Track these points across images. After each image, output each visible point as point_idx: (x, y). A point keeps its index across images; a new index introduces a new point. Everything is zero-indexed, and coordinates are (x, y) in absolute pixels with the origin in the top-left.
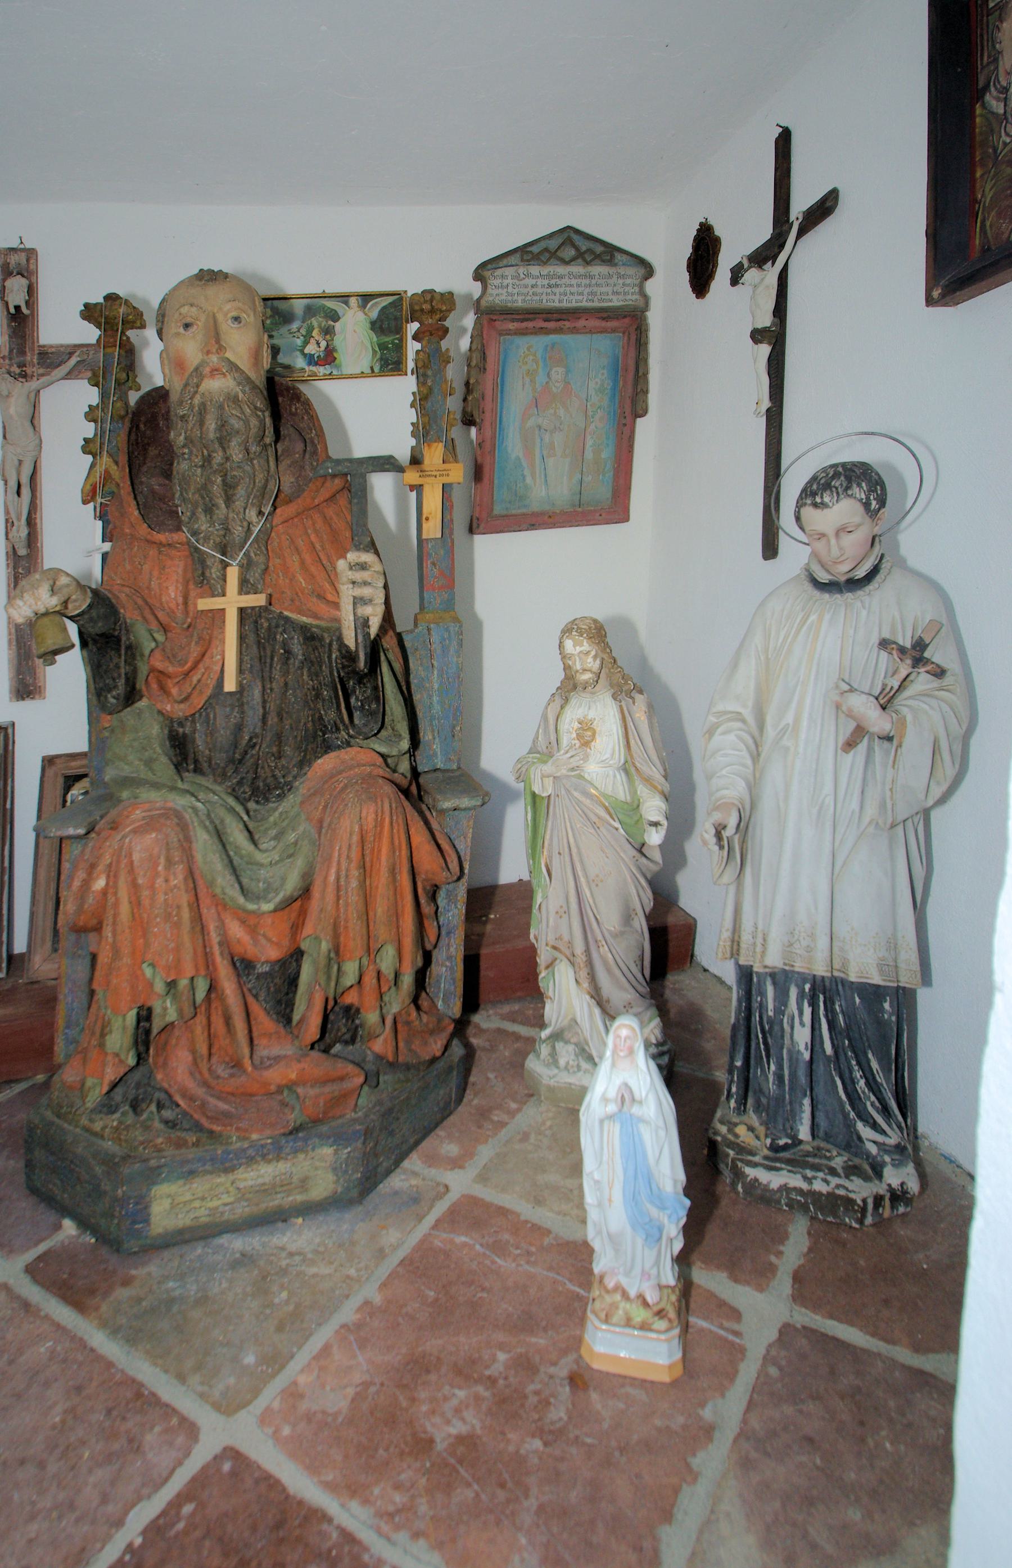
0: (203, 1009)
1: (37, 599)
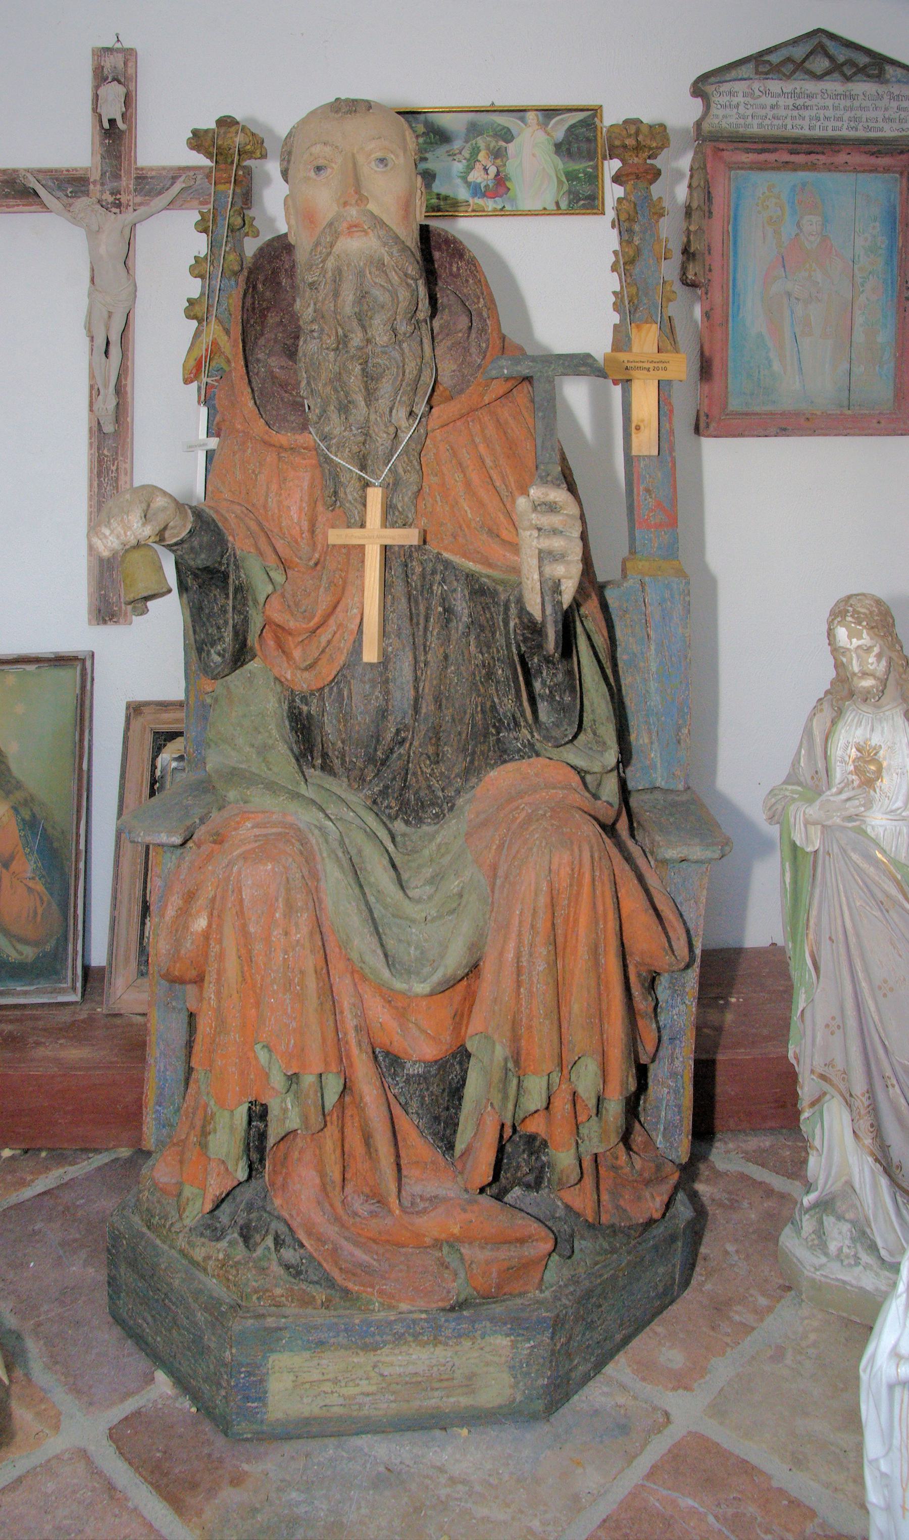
0: (335, 1117)
1: (127, 527)
